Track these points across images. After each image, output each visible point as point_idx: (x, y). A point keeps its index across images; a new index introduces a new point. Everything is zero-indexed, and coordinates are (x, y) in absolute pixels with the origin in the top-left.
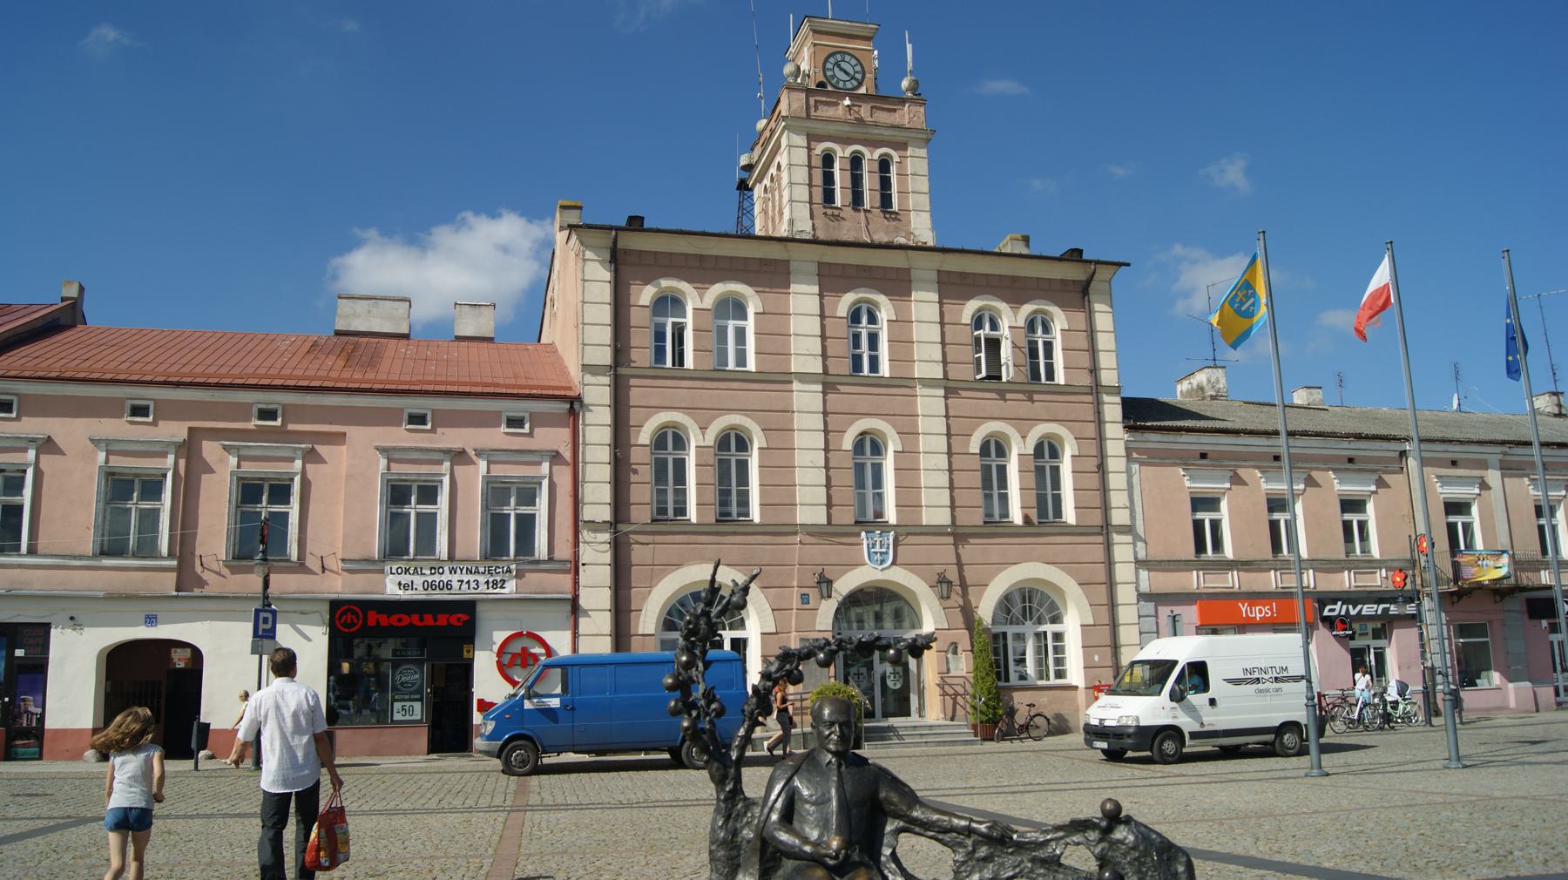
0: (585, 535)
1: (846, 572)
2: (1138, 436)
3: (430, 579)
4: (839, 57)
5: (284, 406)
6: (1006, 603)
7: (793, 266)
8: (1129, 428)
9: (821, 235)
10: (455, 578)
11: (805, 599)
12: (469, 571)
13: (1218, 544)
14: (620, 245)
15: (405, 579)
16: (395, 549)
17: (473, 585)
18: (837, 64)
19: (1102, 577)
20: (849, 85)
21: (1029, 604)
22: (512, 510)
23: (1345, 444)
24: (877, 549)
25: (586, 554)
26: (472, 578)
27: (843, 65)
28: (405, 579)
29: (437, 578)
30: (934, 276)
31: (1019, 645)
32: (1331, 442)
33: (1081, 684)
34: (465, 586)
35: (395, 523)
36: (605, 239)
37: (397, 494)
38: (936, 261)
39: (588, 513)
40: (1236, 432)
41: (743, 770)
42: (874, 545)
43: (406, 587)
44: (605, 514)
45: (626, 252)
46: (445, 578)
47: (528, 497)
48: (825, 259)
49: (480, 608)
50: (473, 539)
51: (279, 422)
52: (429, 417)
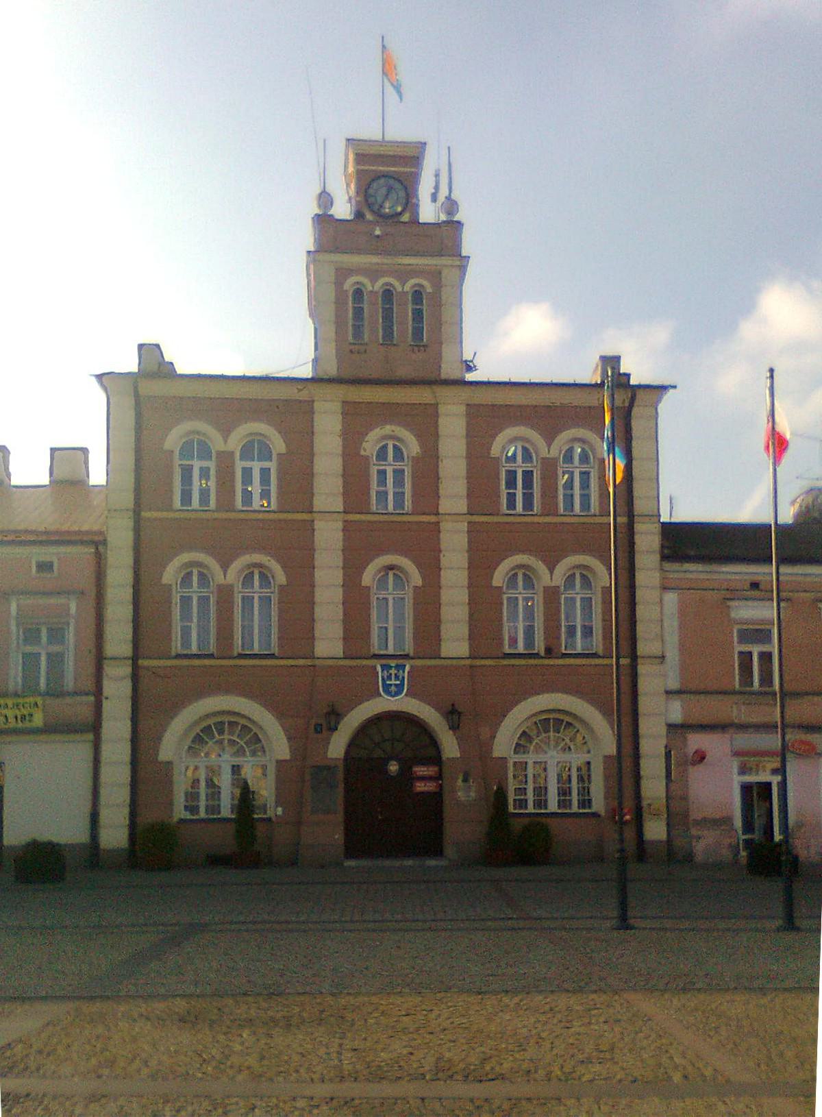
18: (390, 188)
44: (127, 650)
48: (476, 401)
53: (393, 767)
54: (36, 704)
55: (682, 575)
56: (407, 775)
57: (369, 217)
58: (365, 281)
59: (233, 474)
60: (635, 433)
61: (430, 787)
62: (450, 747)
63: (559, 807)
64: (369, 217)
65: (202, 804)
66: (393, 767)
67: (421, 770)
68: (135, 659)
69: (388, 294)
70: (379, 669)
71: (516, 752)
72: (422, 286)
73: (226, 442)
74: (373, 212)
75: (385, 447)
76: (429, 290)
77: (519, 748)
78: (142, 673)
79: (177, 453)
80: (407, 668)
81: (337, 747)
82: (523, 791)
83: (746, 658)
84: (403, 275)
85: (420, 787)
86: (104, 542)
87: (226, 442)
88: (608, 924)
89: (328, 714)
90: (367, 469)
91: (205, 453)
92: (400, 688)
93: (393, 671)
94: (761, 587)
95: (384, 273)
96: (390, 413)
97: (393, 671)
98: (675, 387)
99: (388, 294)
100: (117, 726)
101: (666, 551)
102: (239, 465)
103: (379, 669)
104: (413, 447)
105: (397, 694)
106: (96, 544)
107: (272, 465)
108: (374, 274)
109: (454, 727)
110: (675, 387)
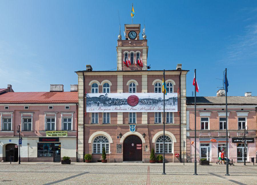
0: (79, 127)
1: (126, 132)
2: (189, 106)
3: (53, 134)
4: (132, 32)
5: (29, 106)
6: (158, 140)
7: (118, 76)
8: (187, 104)
9: (124, 70)
10: (57, 134)
11: (118, 137)
12: (59, 133)
13: (207, 127)
14: (85, 75)
15: (49, 134)
16: (48, 129)
17: (60, 135)
18: (132, 34)
19: (179, 134)
20: (133, 38)
21: (164, 138)
22: (67, 122)
23: (240, 106)
24: (132, 128)
25: (79, 130)
26: (60, 134)
27: (133, 34)
28: (49, 134)
29: (54, 134)
30: (122, 76)
31: (242, 145)
32: (237, 106)
33: (173, 153)
34: (59, 135)
35: (49, 125)
36: (81, 74)
37: (48, 120)
38: (147, 73)
39: (79, 123)
40: (213, 105)
41: (165, 163)
42: (132, 128)
43: (49, 135)
44: (82, 123)
45: (86, 76)
46: (56, 134)
47: (70, 120)
48: (124, 74)
49: (60, 139)
50: (61, 127)
51: (28, 109)
52: (28, 107)
53: (133, 145)
54: (66, 133)
55: (190, 108)
56: (135, 146)
57: (129, 39)
58: (133, 52)
59: (102, 90)
60: (181, 80)
61: (140, 148)
62: (143, 141)
63: (94, 153)
64: (129, 39)
65: (159, 150)
66: (133, 145)
67: (138, 145)
68: (84, 124)
69: (132, 54)
70: (130, 126)
71: (94, 142)
72: (139, 52)
73: (100, 84)
74: (130, 38)
75: (169, 83)
76: (140, 53)
77: (157, 141)
78: (85, 127)
79: (103, 86)
80: (135, 126)
81: (122, 141)
82: (158, 149)
83: (221, 124)
84: (135, 50)
85: (138, 148)
86: (78, 103)
87: (100, 84)
88: (161, 173)
89: (120, 135)
90: (128, 88)
91: (97, 86)
92: (134, 130)
93: (133, 127)
94: (206, 109)
95: (137, 50)
96: (133, 77)
97: (133, 127)
98: (189, 71)
99: (132, 54)
100: (81, 137)
101: (187, 103)
102: (103, 88)
103: (130, 126)
104: (137, 84)
105: (133, 131)
106: (76, 103)
107: (109, 88)
108: (129, 50)
109: (144, 137)
110: (189, 71)
